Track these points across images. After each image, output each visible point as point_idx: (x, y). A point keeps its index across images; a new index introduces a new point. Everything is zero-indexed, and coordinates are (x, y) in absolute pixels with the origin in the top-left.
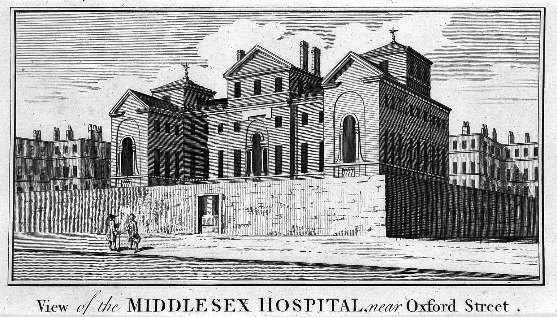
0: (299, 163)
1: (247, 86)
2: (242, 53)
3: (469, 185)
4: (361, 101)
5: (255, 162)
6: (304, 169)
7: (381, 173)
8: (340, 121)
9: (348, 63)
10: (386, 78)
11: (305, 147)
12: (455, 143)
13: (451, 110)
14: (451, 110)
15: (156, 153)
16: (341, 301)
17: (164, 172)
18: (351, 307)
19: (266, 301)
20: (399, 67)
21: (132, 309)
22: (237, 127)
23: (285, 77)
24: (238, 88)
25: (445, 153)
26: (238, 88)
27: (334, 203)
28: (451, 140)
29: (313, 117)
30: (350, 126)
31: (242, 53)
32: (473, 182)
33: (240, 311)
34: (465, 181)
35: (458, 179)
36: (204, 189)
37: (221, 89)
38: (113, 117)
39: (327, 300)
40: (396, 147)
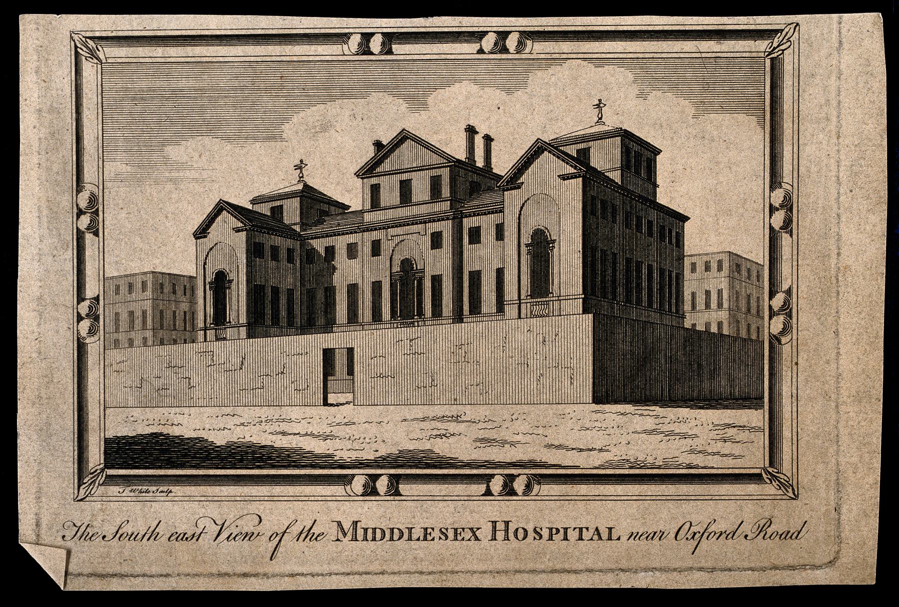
0: (468, 298)
1: (390, 195)
2: (378, 145)
3: (714, 329)
4: (559, 208)
5: (408, 298)
6: (475, 309)
7: (585, 311)
8: (526, 239)
9: (537, 150)
10: (591, 178)
11: (476, 277)
12: (694, 265)
13: (687, 218)
14: (687, 218)
15: (256, 294)
16: (592, 531)
17: (266, 316)
18: (605, 535)
19: (500, 526)
20: (606, 159)
21: (341, 536)
22: (376, 248)
23: (445, 173)
24: (375, 190)
25: (680, 277)
26: (375, 190)
27: (622, 529)
28: (687, 262)
29: (488, 235)
30: (541, 247)
31: (378, 145)
32: (720, 325)
33: (592, 539)
34: (708, 325)
35: (697, 319)
36: (335, 340)
37: (351, 194)
38: (197, 238)
39: (619, 539)
40: (609, 284)
